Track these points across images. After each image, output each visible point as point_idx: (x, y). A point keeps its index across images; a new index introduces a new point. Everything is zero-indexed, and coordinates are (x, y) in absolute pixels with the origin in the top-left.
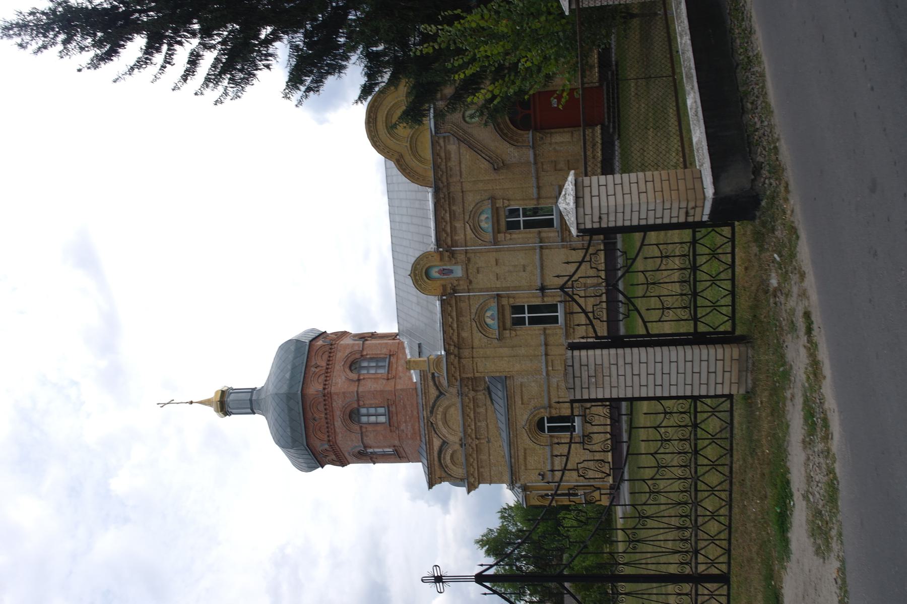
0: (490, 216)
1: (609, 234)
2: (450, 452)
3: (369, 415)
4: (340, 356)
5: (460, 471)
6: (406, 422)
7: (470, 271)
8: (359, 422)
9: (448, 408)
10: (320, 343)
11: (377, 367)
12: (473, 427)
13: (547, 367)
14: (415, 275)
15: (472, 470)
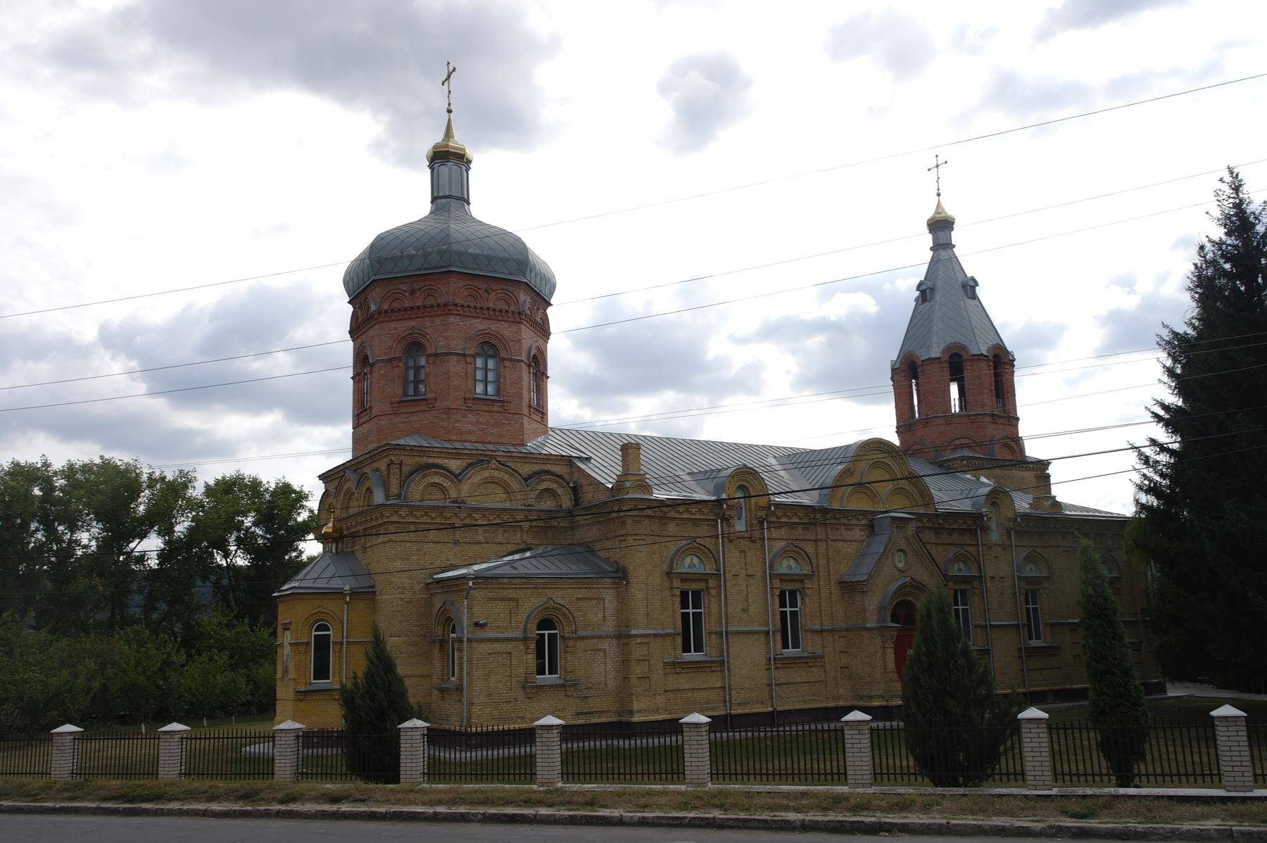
0: (793, 571)
1: (274, 737)
2: (446, 483)
3: (486, 370)
4: (505, 329)
5: (418, 496)
6: (478, 422)
8: (479, 355)
10: (523, 297)
12: (480, 522)
13: (642, 636)
14: (744, 473)
15: (418, 514)
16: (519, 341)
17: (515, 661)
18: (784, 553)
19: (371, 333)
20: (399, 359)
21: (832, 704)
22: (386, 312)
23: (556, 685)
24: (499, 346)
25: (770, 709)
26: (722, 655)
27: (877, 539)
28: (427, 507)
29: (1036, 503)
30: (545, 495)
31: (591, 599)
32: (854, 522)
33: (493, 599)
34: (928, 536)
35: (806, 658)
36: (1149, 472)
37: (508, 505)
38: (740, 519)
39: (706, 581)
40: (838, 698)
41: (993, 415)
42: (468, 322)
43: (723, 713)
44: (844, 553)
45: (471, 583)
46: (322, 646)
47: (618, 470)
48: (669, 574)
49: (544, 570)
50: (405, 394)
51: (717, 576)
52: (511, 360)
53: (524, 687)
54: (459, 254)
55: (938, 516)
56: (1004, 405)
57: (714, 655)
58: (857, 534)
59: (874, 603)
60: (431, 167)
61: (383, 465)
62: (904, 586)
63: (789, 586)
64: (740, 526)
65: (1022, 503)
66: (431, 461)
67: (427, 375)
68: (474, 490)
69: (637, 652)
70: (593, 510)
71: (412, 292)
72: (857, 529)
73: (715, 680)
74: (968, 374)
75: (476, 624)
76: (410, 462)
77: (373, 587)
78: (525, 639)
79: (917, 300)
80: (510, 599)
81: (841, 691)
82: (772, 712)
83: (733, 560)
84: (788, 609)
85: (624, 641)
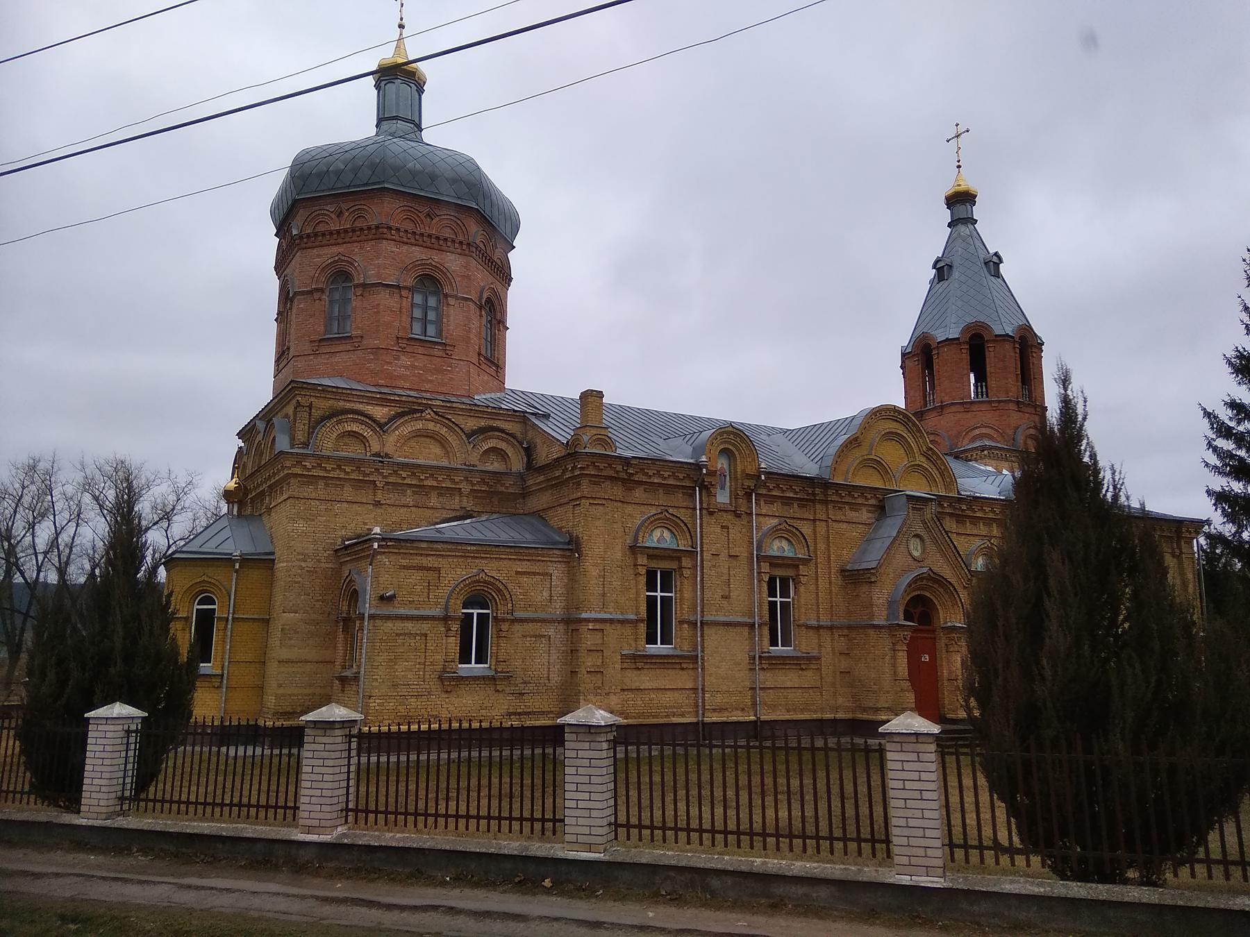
0: (786, 554)
2: (367, 433)
6: (413, 367)
7: (725, 515)
9: (442, 442)
12: (408, 481)
13: (596, 620)
14: (728, 433)
15: (329, 467)
17: (431, 646)
18: (776, 533)
20: (322, 290)
22: (308, 236)
23: (484, 678)
25: (753, 718)
26: (695, 649)
27: (889, 521)
28: (341, 459)
31: (535, 574)
32: (860, 501)
33: (405, 568)
34: (950, 524)
35: (797, 658)
36: (1227, 445)
38: (723, 488)
39: (679, 559)
41: (1018, 403)
43: (694, 720)
44: (845, 538)
45: (376, 545)
48: (634, 549)
49: (476, 535)
50: (327, 331)
51: (692, 554)
52: (456, 297)
53: (441, 678)
54: (396, 169)
55: (960, 500)
56: (1030, 392)
57: (686, 649)
58: (865, 515)
59: (885, 597)
62: (919, 578)
64: (723, 497)
66: (348, 405)
69: (589, 640)
71: (340, 215)
72: (864, 510)
73: (684, 679)
75: (382, 598)
76: (322, 405)
77: (273, 553)
78: (446, 619)
79: (932, 282)
80: (429, 569)
81: (840, 700)
82: (755, 722)
83: (712, 536)
84: (659, 594)
85: (573, 626)
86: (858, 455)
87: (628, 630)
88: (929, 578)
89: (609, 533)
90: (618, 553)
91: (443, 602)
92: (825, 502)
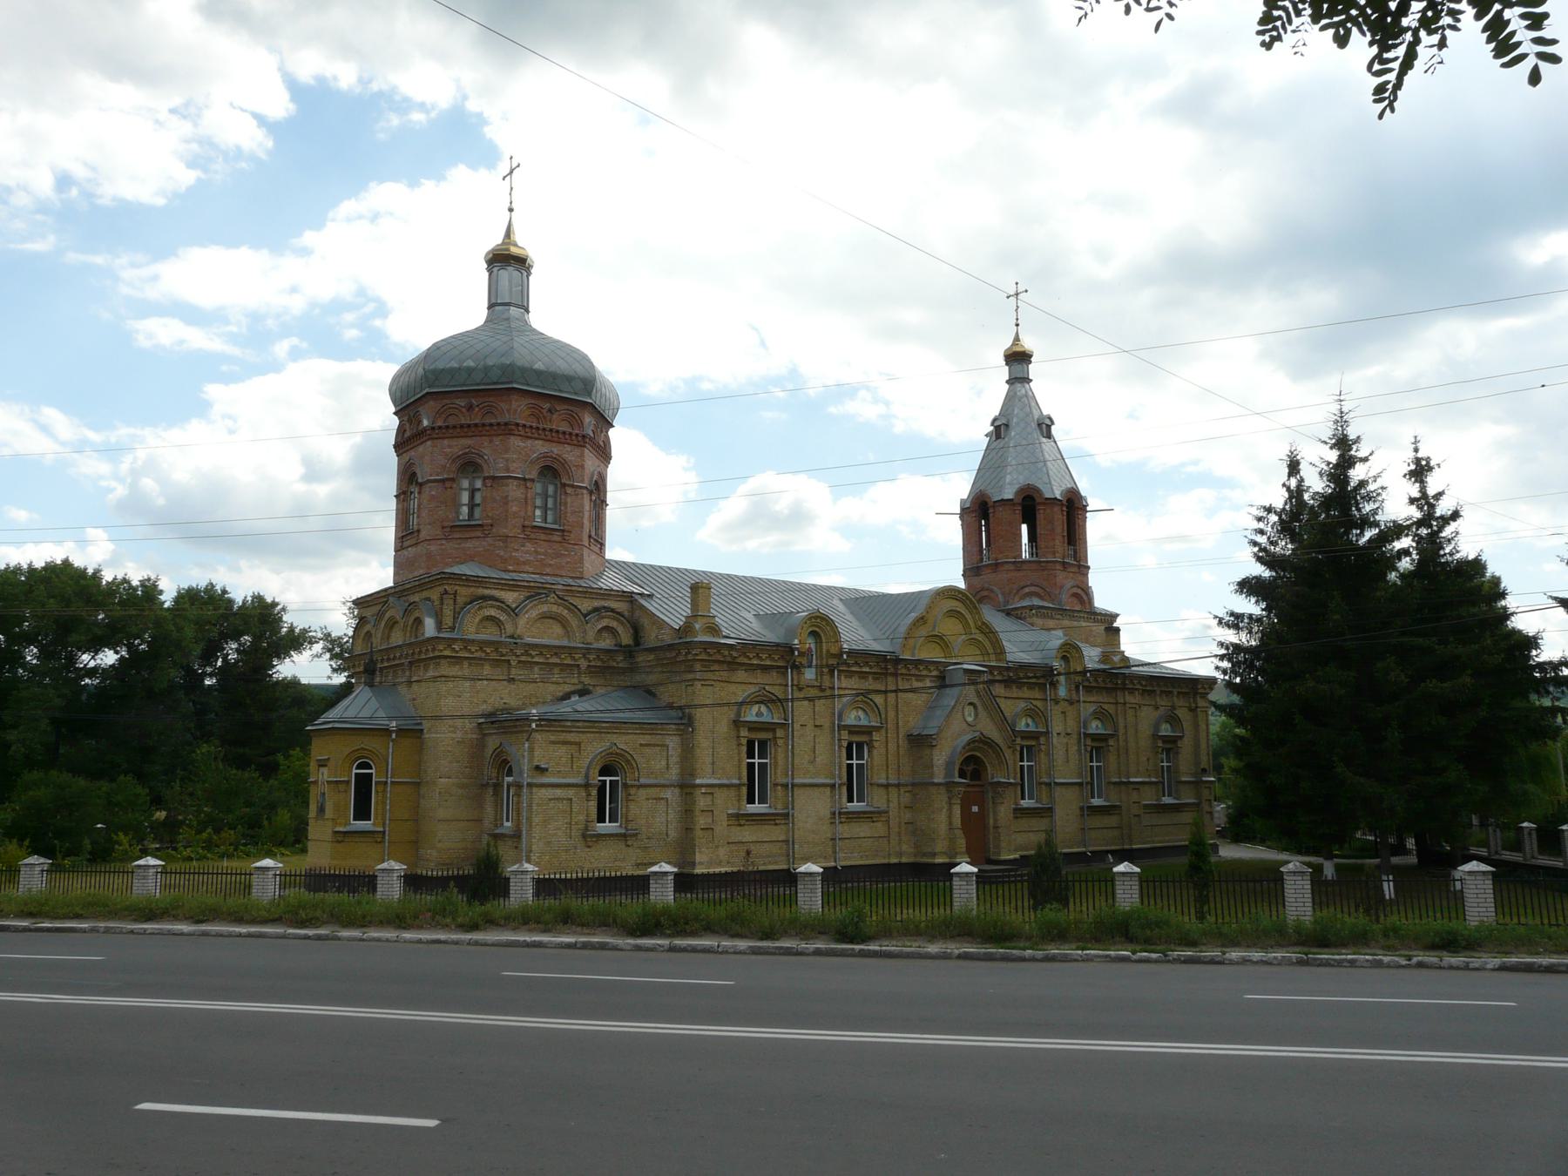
4: (568, 453)
10: (588, 419)
11: (545, 509)
16: (582, 467)
17: (575, 808)
19: (421, 449)
21: (894, 860)
24: (560, 470)
29: (1105, 658)
30: (605, 634)
33: (553, 743)
34: (999, 690)
37: (565, 643)
40: (900, 854)
42: (529, 442)
44: (911, 708)
46: (364, 784)
47: (687, 610)
48: (737, 723)
53: (584, 836)
54: (524, 370)
55: (1008, 669)
57: (1045, 803)
60: (490, 271)
61: (434, 595)
62: (972, 741)
63: (856, 738)
64: (1062, 692)
65: (1091, 656)
66: (487, 592)
67: (484, 499)
68: (532, 628)
69: (702, 802)
70: (659, 649)
71: (470, 408)
74: (1040, 517)
75: (538, 768)
78: (587, 786)
80: (571, 743)
81: (904, 847)
84: (756, 761)
86: (923, 631)
87: (733, 792)
88: (980, 741)
89: (717, 705)
90: (723, 727)
91: (583, 771)
92: (895, 675)
